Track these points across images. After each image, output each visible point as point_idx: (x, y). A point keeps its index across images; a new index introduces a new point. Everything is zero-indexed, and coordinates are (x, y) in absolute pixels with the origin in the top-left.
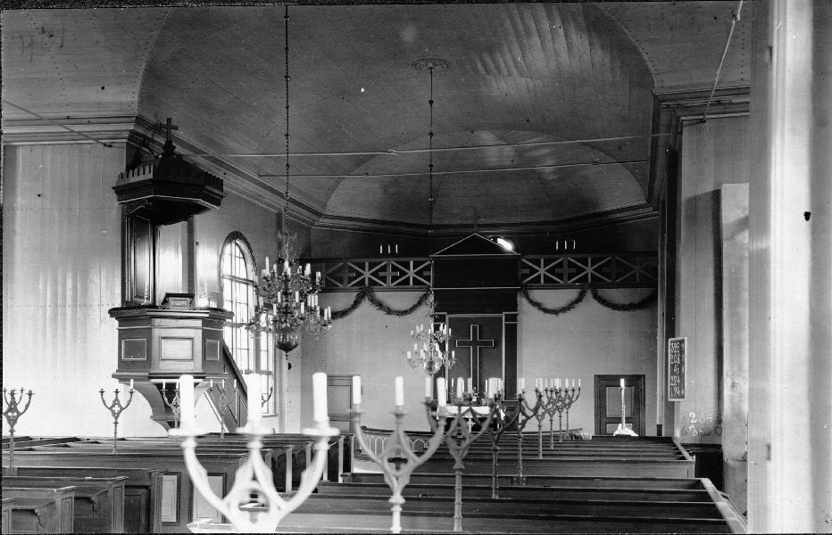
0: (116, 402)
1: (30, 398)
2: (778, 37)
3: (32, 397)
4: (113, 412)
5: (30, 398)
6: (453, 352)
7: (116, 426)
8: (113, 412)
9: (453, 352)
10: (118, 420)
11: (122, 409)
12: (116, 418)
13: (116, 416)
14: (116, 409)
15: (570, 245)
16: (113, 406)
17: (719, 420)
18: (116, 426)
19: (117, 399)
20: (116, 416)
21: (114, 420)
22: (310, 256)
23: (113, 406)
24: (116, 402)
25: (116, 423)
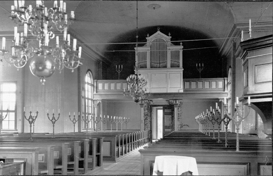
0: (54, 118)
1: (59, 116)
2: (245, 153)
3: (54, 115)
4: (52, 122)
5: (59, 116)
6: (80, 48)
7: (54, 127)
8: (73, 122)
9: (80, 48)
10: (54, 125)
11: (56, 120)
12: (74, 124)
13: (54, 123)
14: (31, 120)
15: (201, 65)
16: (52, 119)
17: (256, 129)
18: (54, 127)
19: (54, 117)
20: (54, 123)
21: (30, 125)
22: (15, 44)
23: (52, 119)
24: (54, 118)
25: (54, 126)
